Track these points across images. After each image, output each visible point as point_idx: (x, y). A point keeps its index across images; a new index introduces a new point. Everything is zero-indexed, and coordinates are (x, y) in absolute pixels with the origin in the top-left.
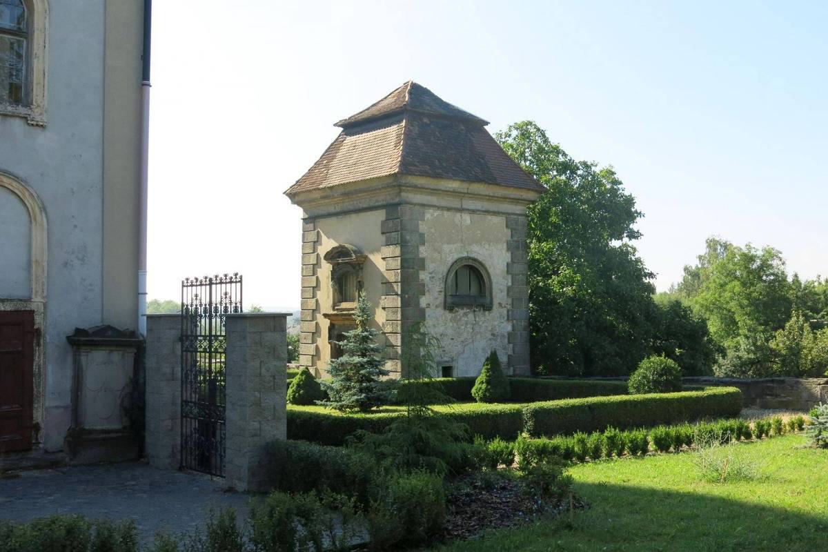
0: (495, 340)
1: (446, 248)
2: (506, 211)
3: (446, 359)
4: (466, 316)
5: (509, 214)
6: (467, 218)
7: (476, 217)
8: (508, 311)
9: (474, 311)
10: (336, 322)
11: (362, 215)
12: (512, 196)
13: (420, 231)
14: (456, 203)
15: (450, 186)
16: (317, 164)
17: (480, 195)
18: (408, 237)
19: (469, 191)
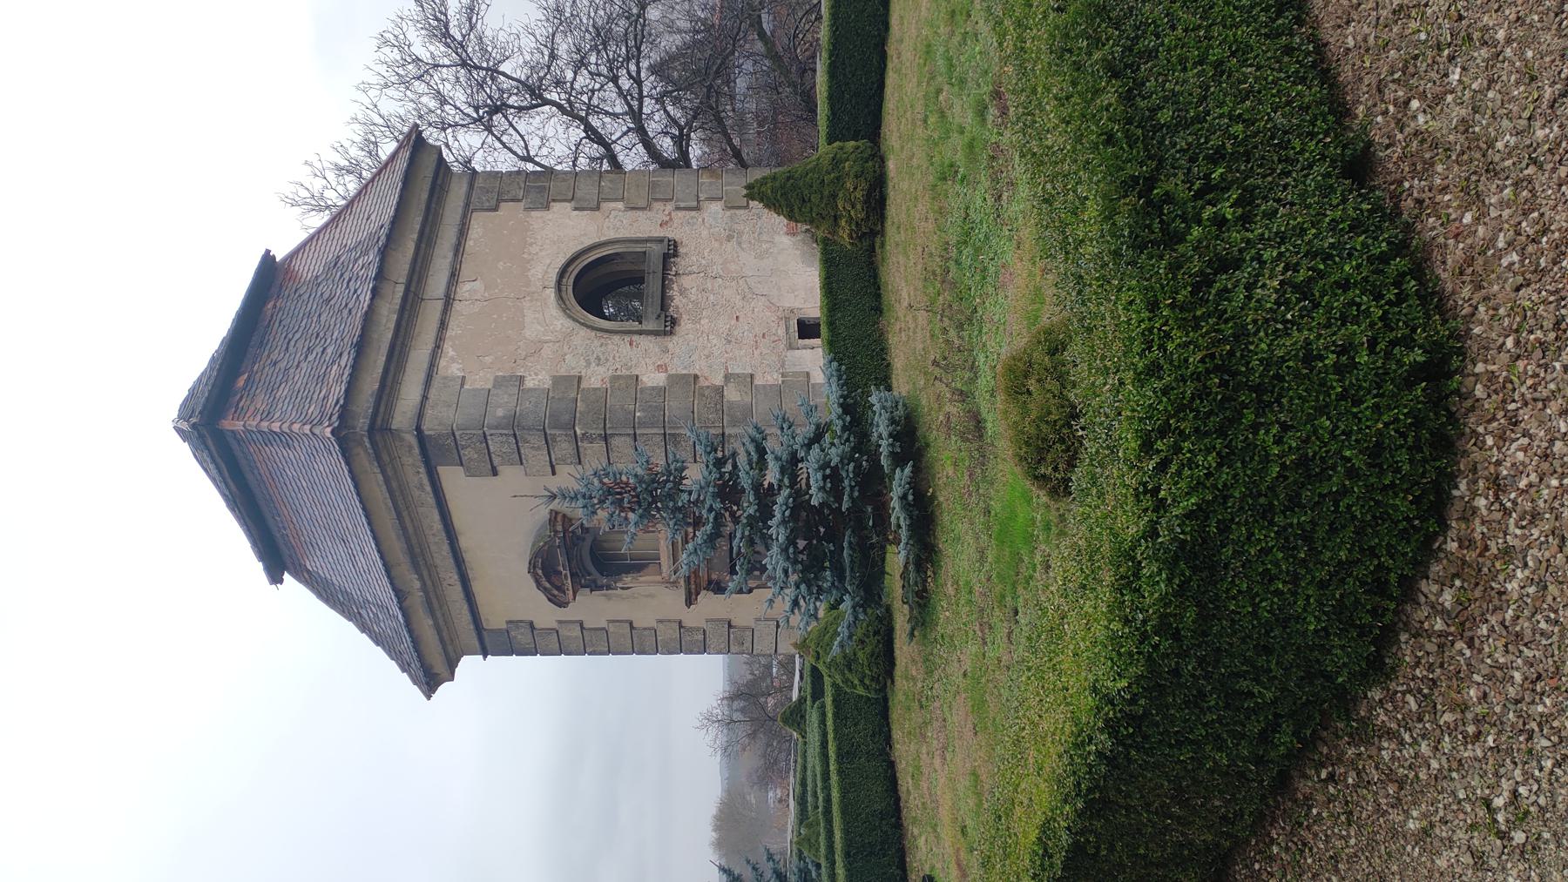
0: (740, 234)
1: (532, 331)
3: (781, 332)
4: (687, 292)
5: (467, 205)
7: (466, 270)
8: (678, 208)
9: (677, 274)
11: (459, 520)
13: (489, 386)
16: (364, 628)
18: (500, 413)
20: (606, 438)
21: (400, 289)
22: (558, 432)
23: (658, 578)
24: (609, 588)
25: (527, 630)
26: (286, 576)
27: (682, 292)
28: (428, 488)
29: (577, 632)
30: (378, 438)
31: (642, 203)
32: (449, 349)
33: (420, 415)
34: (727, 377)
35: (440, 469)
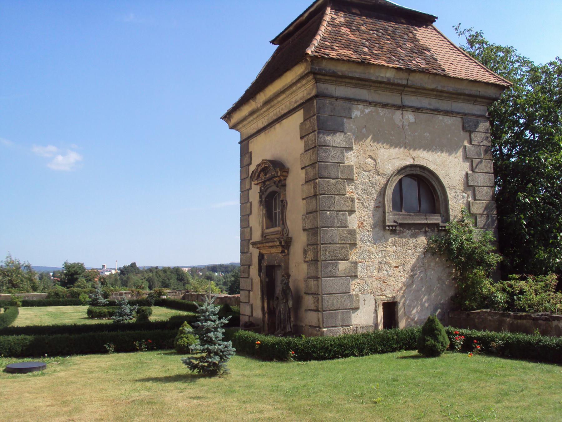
2: (462, 111)
5: (465, 114)
6: (410, 117)
7: (422, 116)
10: (264, 251)
12: (467, 92)
14: (396, 99)
15: (383, 75)
17: (425, 89)
19: (410, 83)
20: (315, 196)
22: (317, 169)
23: (265, 228)
26: (277, 47)
28: (295, 105)
30: (311, 77)
34: (356, 263)
35: (302, 111)
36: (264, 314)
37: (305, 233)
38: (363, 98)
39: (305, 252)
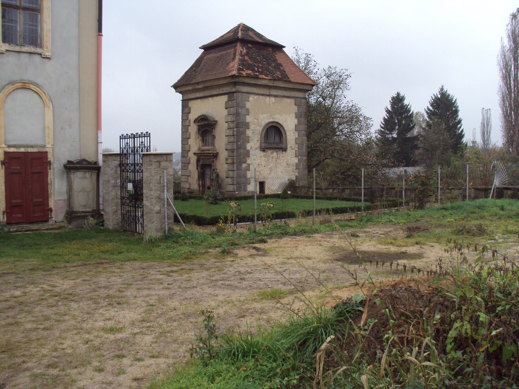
0: (289, 167)
1: (262, 116)
5: (296, 98)
6: (273, 99)
7: (278, 99)
8: (296, 151)
11: (215, 98)
21: (272, 85)
24: (198, 133)
25: (188, 111)
27: (272, 153)
28: (223, 92)
29: (187, 124)
31: (297, 142)
32: (256, 97)
33: (239, 92)
34: (249, 165)
35: (227, 96)
36: (199, 187)
37: (227, 151)
38: (253, 92)
39: (227, 159)
